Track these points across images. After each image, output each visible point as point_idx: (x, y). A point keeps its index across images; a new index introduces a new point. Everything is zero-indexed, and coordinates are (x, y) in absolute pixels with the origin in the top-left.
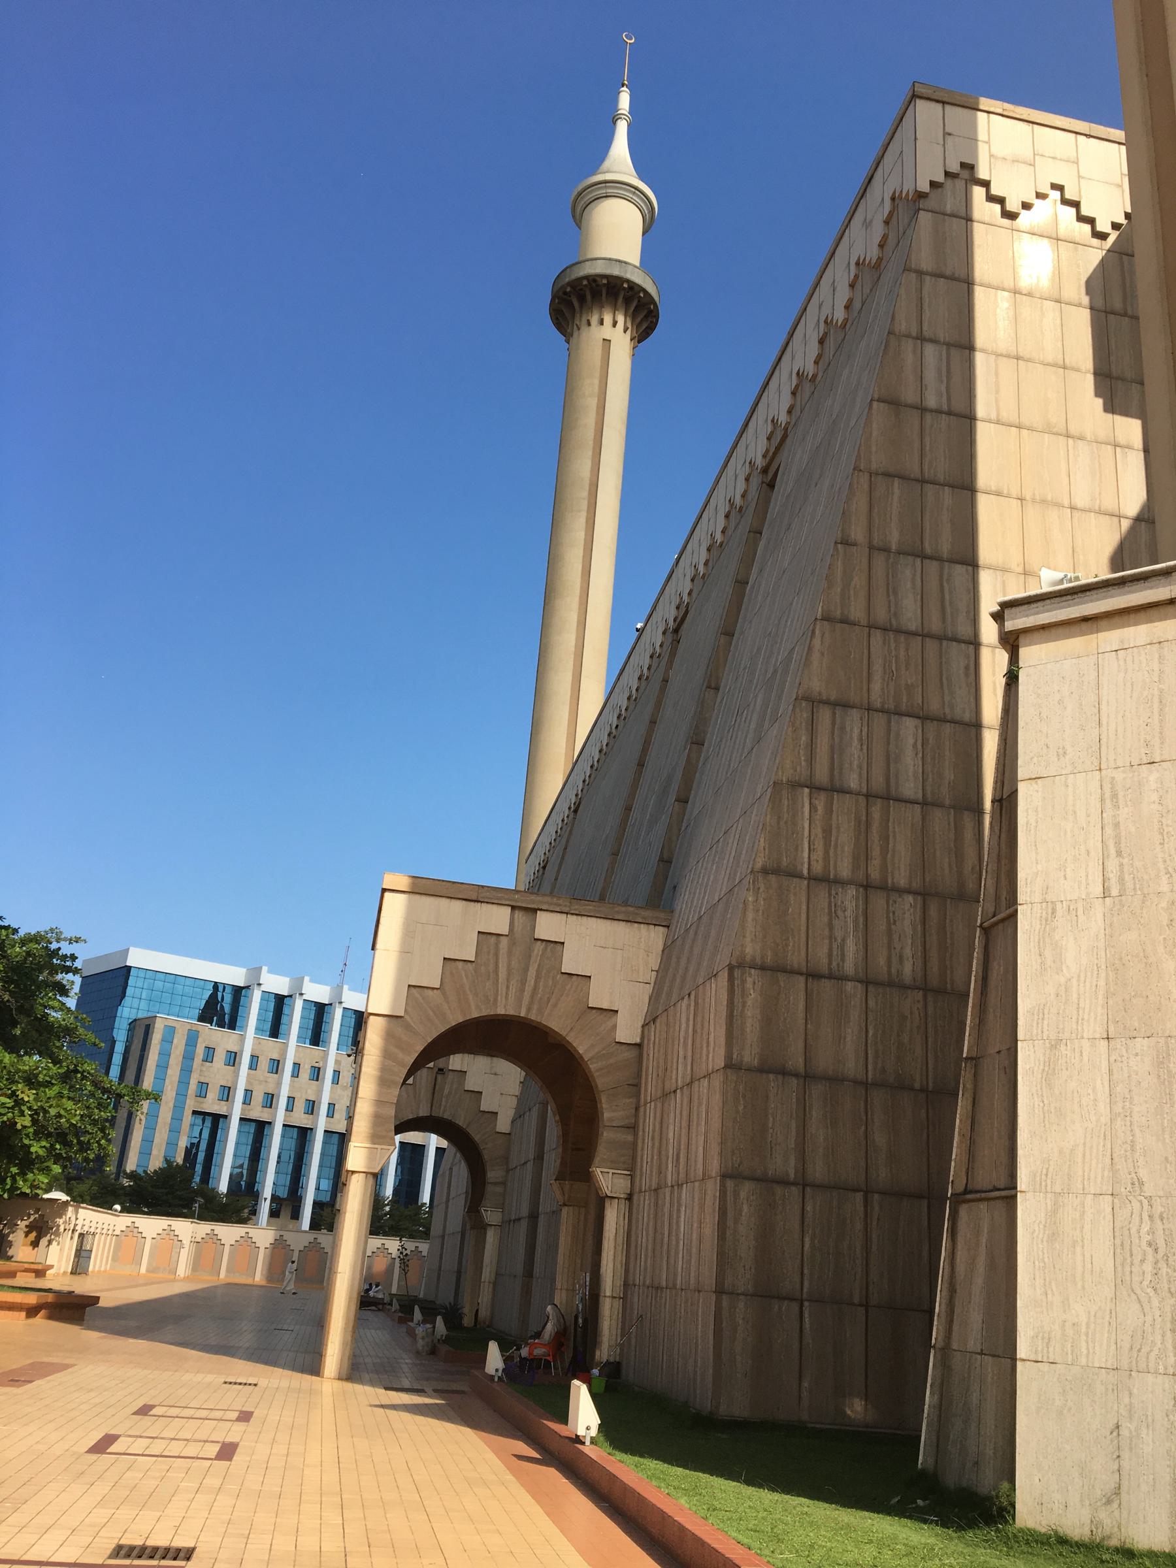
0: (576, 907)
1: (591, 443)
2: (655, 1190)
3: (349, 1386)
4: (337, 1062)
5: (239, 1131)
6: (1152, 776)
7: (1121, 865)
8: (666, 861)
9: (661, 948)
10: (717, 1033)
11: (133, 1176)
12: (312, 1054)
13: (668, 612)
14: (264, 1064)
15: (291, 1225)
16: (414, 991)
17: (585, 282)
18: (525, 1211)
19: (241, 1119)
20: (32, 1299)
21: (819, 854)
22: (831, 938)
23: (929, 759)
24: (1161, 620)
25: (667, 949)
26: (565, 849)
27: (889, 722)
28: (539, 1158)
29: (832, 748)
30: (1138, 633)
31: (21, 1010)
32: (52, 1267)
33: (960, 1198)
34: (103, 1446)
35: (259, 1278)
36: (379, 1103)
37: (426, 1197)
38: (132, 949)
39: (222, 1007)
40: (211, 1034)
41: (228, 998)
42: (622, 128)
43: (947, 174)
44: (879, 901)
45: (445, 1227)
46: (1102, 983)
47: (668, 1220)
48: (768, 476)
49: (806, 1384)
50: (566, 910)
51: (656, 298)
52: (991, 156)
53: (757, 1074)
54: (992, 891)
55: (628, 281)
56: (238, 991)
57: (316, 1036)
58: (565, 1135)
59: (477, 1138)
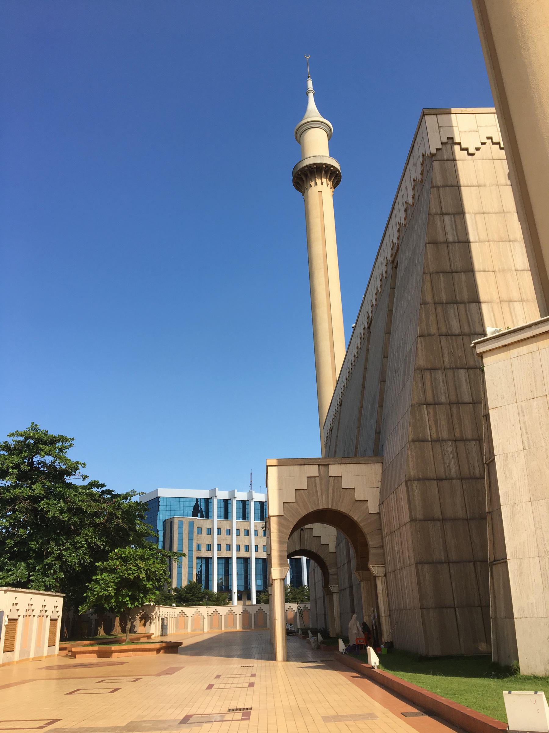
0: (344, 461)
1: (321, 238)
2: (394, 571)
3: (288, 663)
4: (255, 526)
5: (218, 563)
6: (535, 403)
7: (528, 437)
8: (378, 433)
9: (381, 471)
10: (405, 508)
11: (176, 590)
12: (244, 525)
13: (364, 320)
14: (224, 532)
15: (248, 603)
16: (286, 504)
17: (306, 168)
18: (347, 585)
19: (218, 558)
20: (158, 646)
21: (434, 431)
22: (444, 463)
23: (472, 385)
24: (531, 344)
25: (384, 472)
26: (339, 422)
27: (454, 373)
28: (349, 562)
29: (432, 388)
30: (523, 349)
31: (130, 530)
32: (153, 634)
33: (492, 564)
34: (210, 687)
35: (239, 628)
36: (280, 550)
37: (305, 583)
38: (159, 489)
39: (201, 509)
40: (199, 521)
41: (203, 504)
42: (311, 96)
43: (442, 144)
44: (461, 445)
45: (316, 596)
46: (527, 481)
47: (398, 581)
48: (394, 264)
49: (461, 640)
50: (340, 463)
51: (339, 168)
52: (460, 132)
53: (423, 521)
54: (487, 449)
55: (325, 164)
56: (207, 501)
57: (244, 515)
58: (357, 552)
59: (322, 556)
